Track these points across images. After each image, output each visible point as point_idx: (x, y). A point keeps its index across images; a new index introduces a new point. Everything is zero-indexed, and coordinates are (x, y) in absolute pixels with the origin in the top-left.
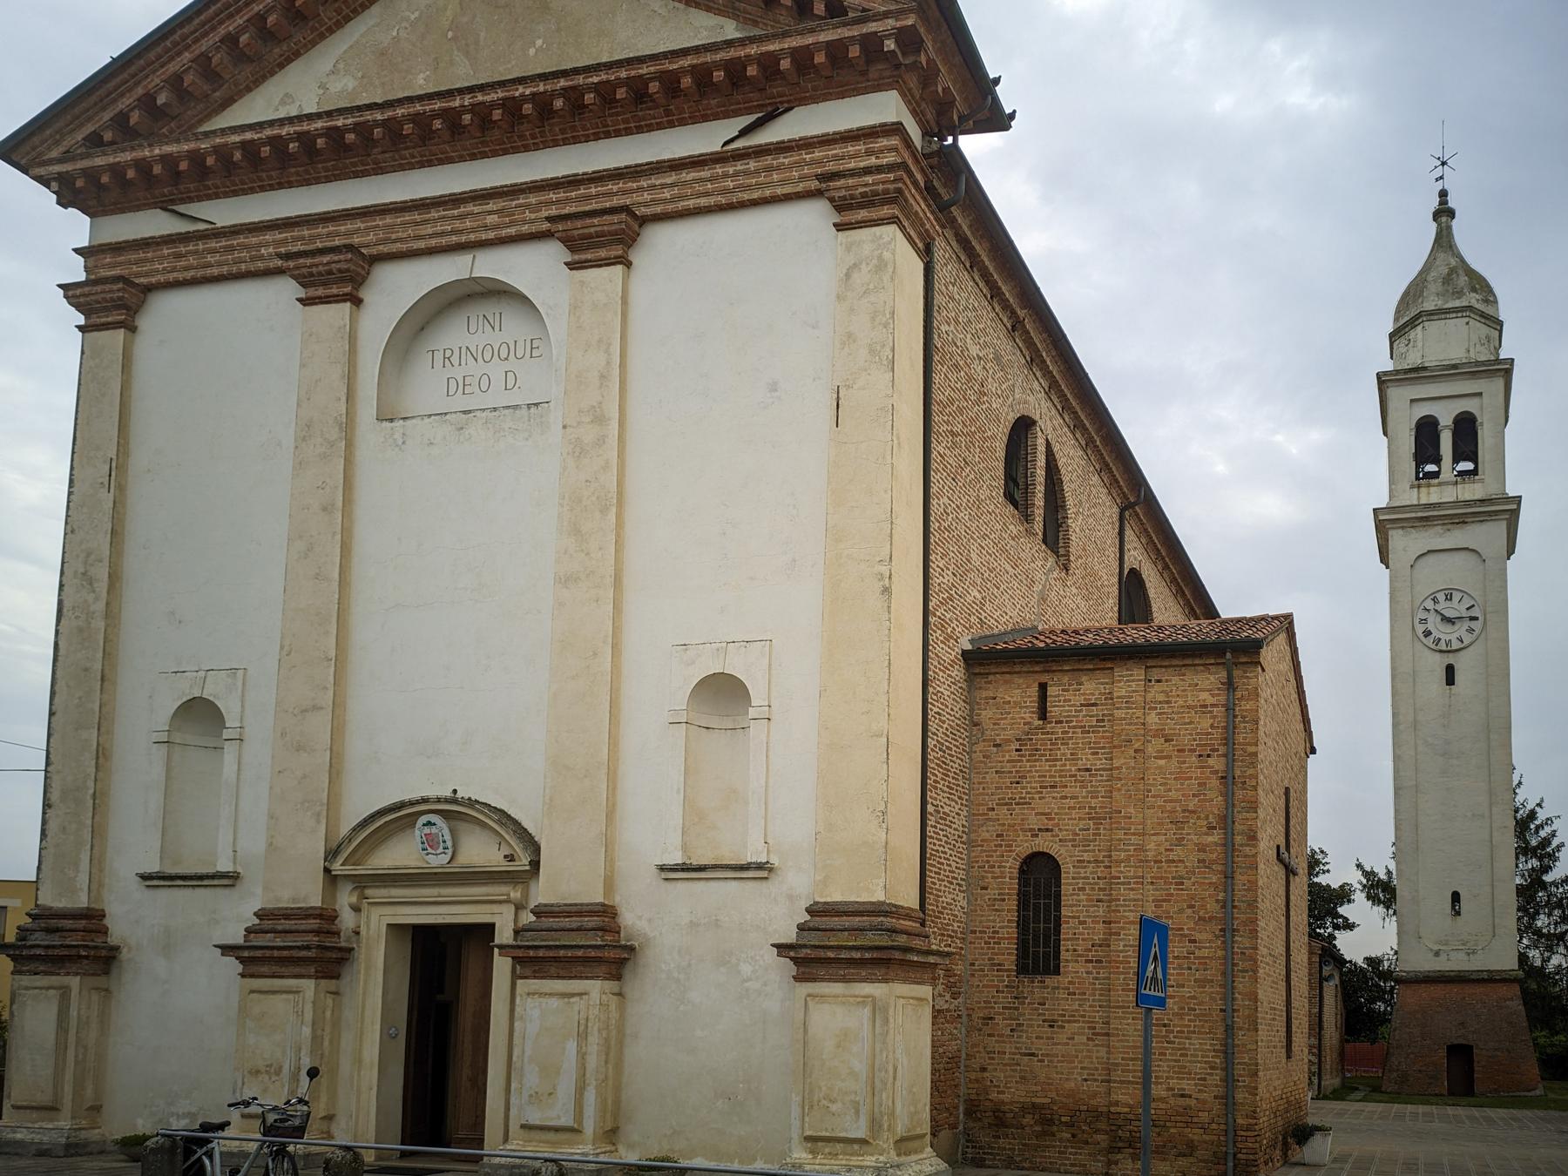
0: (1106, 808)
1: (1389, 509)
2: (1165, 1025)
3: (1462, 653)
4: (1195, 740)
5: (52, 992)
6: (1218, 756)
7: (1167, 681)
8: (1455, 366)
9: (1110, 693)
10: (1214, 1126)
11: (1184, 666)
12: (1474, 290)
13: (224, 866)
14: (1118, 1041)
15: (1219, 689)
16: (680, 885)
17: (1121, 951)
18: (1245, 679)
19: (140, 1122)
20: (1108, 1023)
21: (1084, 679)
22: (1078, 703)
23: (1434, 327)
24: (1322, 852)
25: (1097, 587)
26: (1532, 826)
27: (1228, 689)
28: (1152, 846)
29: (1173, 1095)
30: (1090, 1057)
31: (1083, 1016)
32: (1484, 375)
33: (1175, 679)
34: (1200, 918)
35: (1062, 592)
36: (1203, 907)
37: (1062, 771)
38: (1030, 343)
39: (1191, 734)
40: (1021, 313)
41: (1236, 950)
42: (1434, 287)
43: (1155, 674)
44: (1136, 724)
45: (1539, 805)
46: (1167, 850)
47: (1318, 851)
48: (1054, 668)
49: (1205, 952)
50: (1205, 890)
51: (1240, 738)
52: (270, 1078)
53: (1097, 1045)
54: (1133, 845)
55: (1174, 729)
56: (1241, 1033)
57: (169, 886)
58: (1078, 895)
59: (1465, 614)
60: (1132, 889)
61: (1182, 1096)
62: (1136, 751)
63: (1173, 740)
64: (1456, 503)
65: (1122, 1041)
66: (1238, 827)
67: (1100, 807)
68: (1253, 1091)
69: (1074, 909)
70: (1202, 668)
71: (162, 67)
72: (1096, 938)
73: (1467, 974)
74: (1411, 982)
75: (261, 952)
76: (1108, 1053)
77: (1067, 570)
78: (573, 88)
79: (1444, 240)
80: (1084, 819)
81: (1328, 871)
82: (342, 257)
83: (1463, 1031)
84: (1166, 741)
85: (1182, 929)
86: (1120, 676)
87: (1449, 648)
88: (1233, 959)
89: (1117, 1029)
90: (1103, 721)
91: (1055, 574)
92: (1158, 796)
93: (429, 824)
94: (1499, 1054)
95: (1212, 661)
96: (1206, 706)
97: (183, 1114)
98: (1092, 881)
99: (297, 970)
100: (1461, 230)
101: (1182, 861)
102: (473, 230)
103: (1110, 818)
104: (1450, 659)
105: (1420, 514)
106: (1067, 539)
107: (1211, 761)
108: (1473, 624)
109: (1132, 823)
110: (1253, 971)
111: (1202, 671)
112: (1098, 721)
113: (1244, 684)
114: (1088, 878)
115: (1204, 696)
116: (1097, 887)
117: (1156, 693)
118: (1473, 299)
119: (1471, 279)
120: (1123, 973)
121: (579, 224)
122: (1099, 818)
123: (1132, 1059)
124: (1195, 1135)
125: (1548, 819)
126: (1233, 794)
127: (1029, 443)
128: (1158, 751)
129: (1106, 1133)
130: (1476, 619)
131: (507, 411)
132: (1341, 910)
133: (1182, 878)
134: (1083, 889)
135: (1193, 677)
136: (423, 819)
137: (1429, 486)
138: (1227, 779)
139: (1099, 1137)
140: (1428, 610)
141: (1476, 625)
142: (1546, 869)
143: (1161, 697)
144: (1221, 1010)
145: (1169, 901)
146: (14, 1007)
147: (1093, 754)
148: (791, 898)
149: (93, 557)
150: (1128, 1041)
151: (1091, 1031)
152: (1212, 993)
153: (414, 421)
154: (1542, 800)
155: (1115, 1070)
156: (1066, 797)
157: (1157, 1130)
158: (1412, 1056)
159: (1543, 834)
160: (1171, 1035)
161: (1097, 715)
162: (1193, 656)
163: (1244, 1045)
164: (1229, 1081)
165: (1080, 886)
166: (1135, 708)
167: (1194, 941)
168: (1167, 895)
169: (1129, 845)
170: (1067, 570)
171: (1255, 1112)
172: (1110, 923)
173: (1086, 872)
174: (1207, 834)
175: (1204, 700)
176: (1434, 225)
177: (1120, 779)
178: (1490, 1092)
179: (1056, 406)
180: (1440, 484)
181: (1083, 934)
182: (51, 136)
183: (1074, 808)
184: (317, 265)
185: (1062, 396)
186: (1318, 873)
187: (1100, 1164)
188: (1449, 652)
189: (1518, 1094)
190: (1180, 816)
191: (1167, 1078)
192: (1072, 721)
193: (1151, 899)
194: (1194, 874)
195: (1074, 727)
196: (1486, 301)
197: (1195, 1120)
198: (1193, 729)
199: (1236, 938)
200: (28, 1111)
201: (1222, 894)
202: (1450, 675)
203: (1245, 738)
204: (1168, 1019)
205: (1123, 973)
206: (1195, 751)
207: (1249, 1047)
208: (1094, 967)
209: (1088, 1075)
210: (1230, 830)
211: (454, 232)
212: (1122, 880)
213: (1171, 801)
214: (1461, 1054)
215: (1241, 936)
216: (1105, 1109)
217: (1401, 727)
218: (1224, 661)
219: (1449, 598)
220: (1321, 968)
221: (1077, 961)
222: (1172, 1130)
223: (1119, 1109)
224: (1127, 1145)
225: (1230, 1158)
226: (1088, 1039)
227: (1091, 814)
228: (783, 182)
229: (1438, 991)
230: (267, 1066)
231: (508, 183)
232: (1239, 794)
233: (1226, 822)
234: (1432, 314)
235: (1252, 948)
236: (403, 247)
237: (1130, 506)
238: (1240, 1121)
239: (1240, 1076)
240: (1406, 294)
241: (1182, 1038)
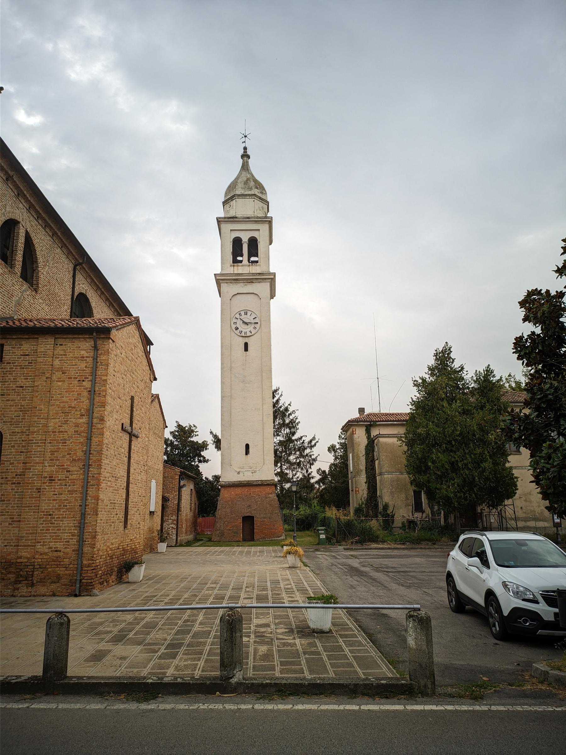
0: (29, 405)
1: (221, 275)
2: (50, 515)
3: (251, 337)
4: (77, 373)
6: (88, 381)
7: (65, 345)
8: (248, 218)
9: (36, 350)
10: (71, 566)
11: (74, 338)
12: (257, 188)
14: (25, 524)
15: (90, 349)
17: (30, 478)
18: (103, 345)
20: (20, 515)
21: (23, 342)
22: (19, 354)
23: (240, 201)
24: (194, 426)
25: (57, 300)
26: (287, 414)
27: (95, 349)
28: (52, 424)
29: (51, 551)
30: (9, 534)
31: (8, 512)
32: (261, 222)
33: (70, 344)
34: (73, 460)
35: (32, 301)
36: (75, 454)
37: (8, 387)
38: (17, 187)
39: (75, 370)
40: (11, 173)
41: (90, 475)
42: (240, 185)
43: (60, 341)
44: (48, 365)
45: (290, 405)
46: (59, 426)
47: (192, 426)
48: (8, 337)
49: (74, 477)
50: (77, 446)
51: (99, 373)
53: (14, 527)
54: (42, 424)
55: (68, 368)
56: (89, 516)
58: (11, 449)
59: (253, 321)
60: (39, 446)
61: (56, 551)
62: (47, 378)
63: (66, 373)
64: (249, 274)
65: (27, 524)
66: (95, 415)
67: (27, 405)
68: (93, 546)
69: (8, 457)
70: (83, 339)
72: (18, 471)
73: (252, 482)
74: (226, 487)
76: (19, 531)
77: (36, 291)
79: (245, 167)
80: (18, 411)
81: (198, 435)
84: (63, 373)
85: (64, 465)
86: (41, 342)
88: (88, 479)
89: (25, 518)
90: (32, 363)
91: (28, 293)
92: (57, 400)
94: (265, 520)
95: (88, 336)
96: (84, 357)
98: (19, 442)
100: (251, 162)
101: (66, 432)
103: (31, 411)
104: (246, 340)
105: (234, 278)
106: (38, 277)
107: (84, 383)
108: (256, 326)
109: (42, 413)
110: (97, 485)
111: (83, 341)
112: (29, 363)
113: (102, 347)
114: (17, 441)
115: (83, 352)
116: (21, 445)
117: (59, 350)
118: (256, 192)
119: (255, 183)
120: (31, 489)
122: (26, 411)
123: (31, 534)
124: (61, 571)
125: (293, 411)
126: (94, 399)
127: (16, 231)
128: (59, 378)
129: (14, 573)
130: (257, 323)
132: (202, 453)
133: (65, 440)
134: (14, 446)
135: (78, 343)
137: (238, 266)
138: (92, 392)
139: (10, 576)
140: (237, 319)
141: (257, 326)
142: (294, 434)
143: (62, 353)
144: (80, 506)
145: (58, 451)
147: (25, 379)
150: (30, 524)
151: (11, 520)
152: (76, 497)
154: (291, 403)
155: (22, 540)
156: (9, 400)
157: (41, 570)
158: (226, 523)
159: (291, 417)
160: (53, 520)
161: (29, 360)
162: (79, 334)
163: (90, 523)
164: (81, 541)
165: (12, 445)
166: (48, 357)
167: (69, 471)
168: (57, 449)
169: (39, 424)
170: (36, 291)
171: (93, 557)
172: (26, 463)
173: (16, 438)
174: (80, 418)
175: (83, 355)
176: (242, 160)
177: (38, 392)
178: (261, 539)
179: (33, 216)
180: (242, 266)
181: (12, 469)
183: (13, 406)
185: (37, 211)
186: (193, 436)
187: (9, 591)
188: (246, 337)
189: (274, 539)
190: (67, 410)
191: (49, 542)
192: (15, 363)
193: (49, 451)
194: (72, 437)
195: (16, 366)
196: (262, 193)
197: (62, 563)
198: (77, 368)
199: (91, 469)
201: (85, 447)
202: (246, 346)
203: (101, 373)
204: (52, 512)
205: (31, 489)
206: (77, 378)
207: (92, 523)
208: (16, 487)
209: (8, 543)
210: (91, 416)
212: (34, 441)
213: (63, 402)
214: (248, 520)
215: (93, 468)
216: (15, 561)
217: (225, 369)
218: (92, 336)
219: (246, 314)
220: (180, 481)
221: (7, 484)
222: (49, 570)
223: (22, 560)
224: (24, 579)
225: (78, 582)
226: (9, 524)
227: (21, 408)
229: (239, 490)
232: (97, 399)
233: (90, 412)
234: (239, 196)
235: (98, 474)
237: (80, 264)
238: (85, 562)
239: (87, 539)
240: (229, 187)
241: (59, 521)
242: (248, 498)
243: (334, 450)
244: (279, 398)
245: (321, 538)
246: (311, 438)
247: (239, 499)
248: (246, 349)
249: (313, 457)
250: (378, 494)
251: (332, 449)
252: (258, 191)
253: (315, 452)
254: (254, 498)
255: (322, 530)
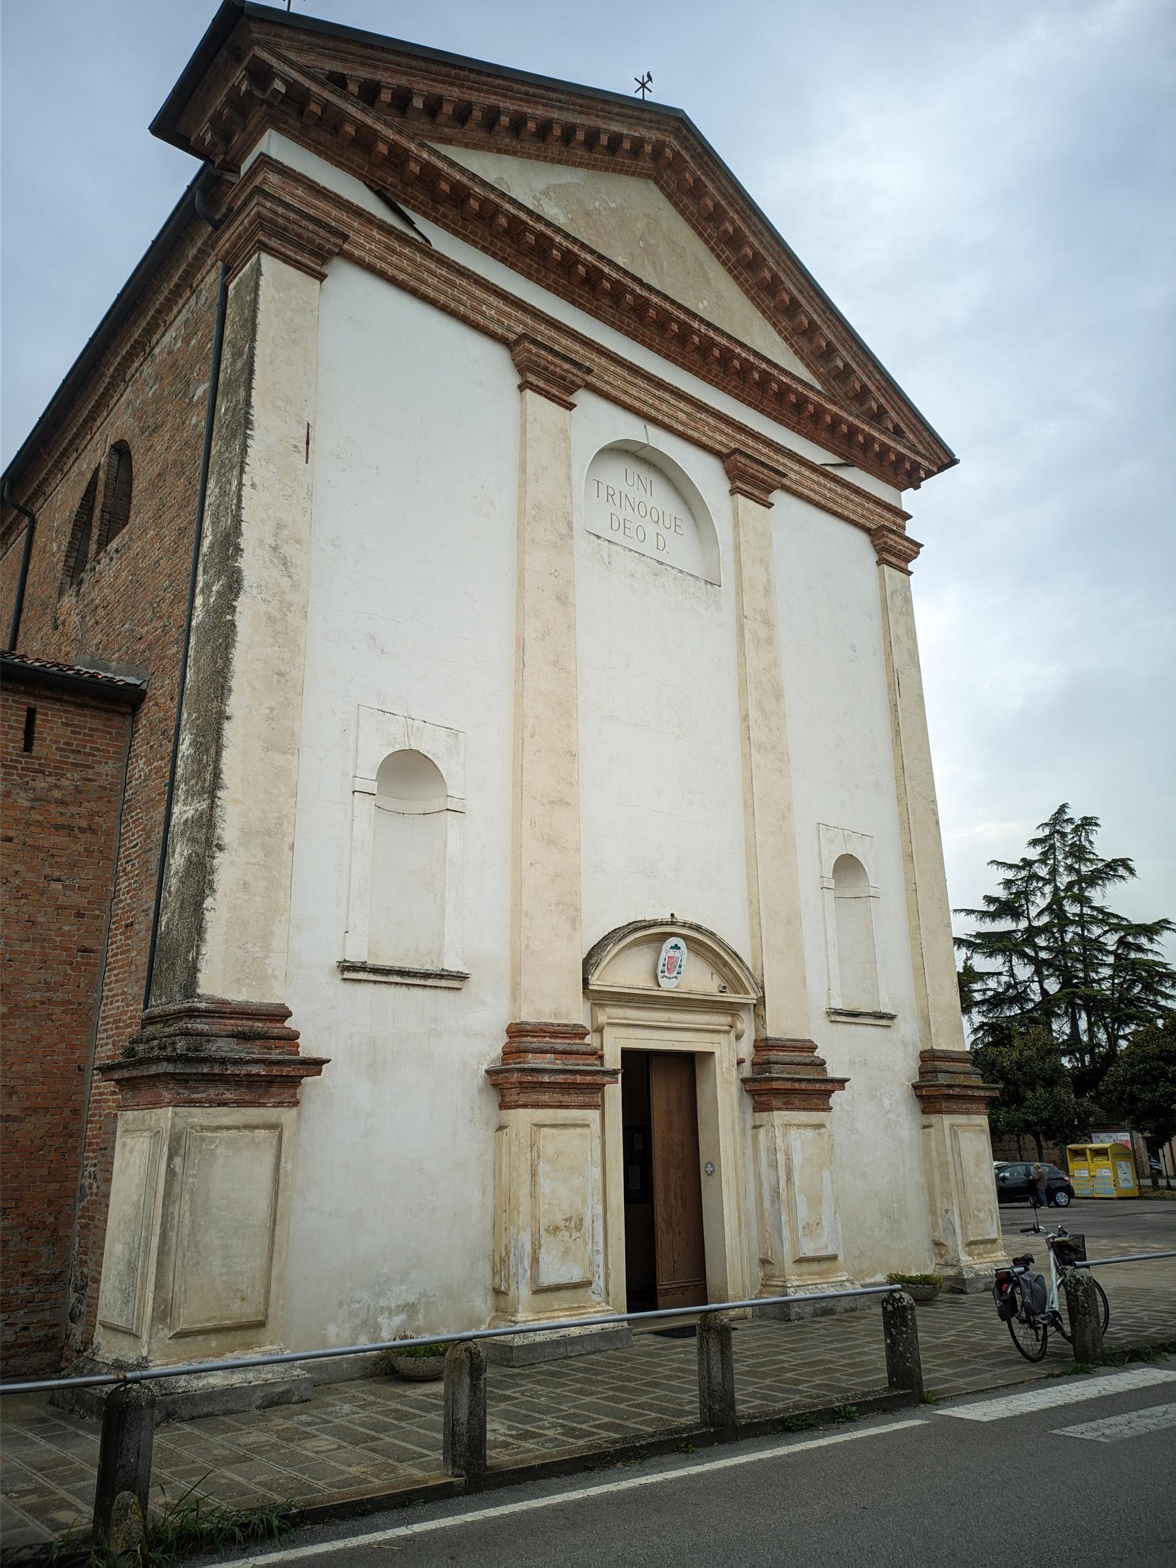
5: (262, 1134)
13: (452, 964)
16: (840, 1026)
19: (332, 1330)
52: (571, 1236)
57: (375, 982)
71: (432, 80)
75: (563, 1077)
78: (770, 374)
82: (580, 374)
93: (676, 947)
97: (398, 1306)
99: (582, 1099)
102: (668, 415)
121: (755, 466)
131: (689, 577)
136: (672, 941)
146: (178, 1160)
148: (904, 1044)
149: (286, 532)
153: (616, 547)
182: (302, 42)
184: (556, 366)
200: (201, 1338)
211: (652, 406)
228: (854, 512)
230: (566, 1220)
231: (704, 401)
236: (606, 388)
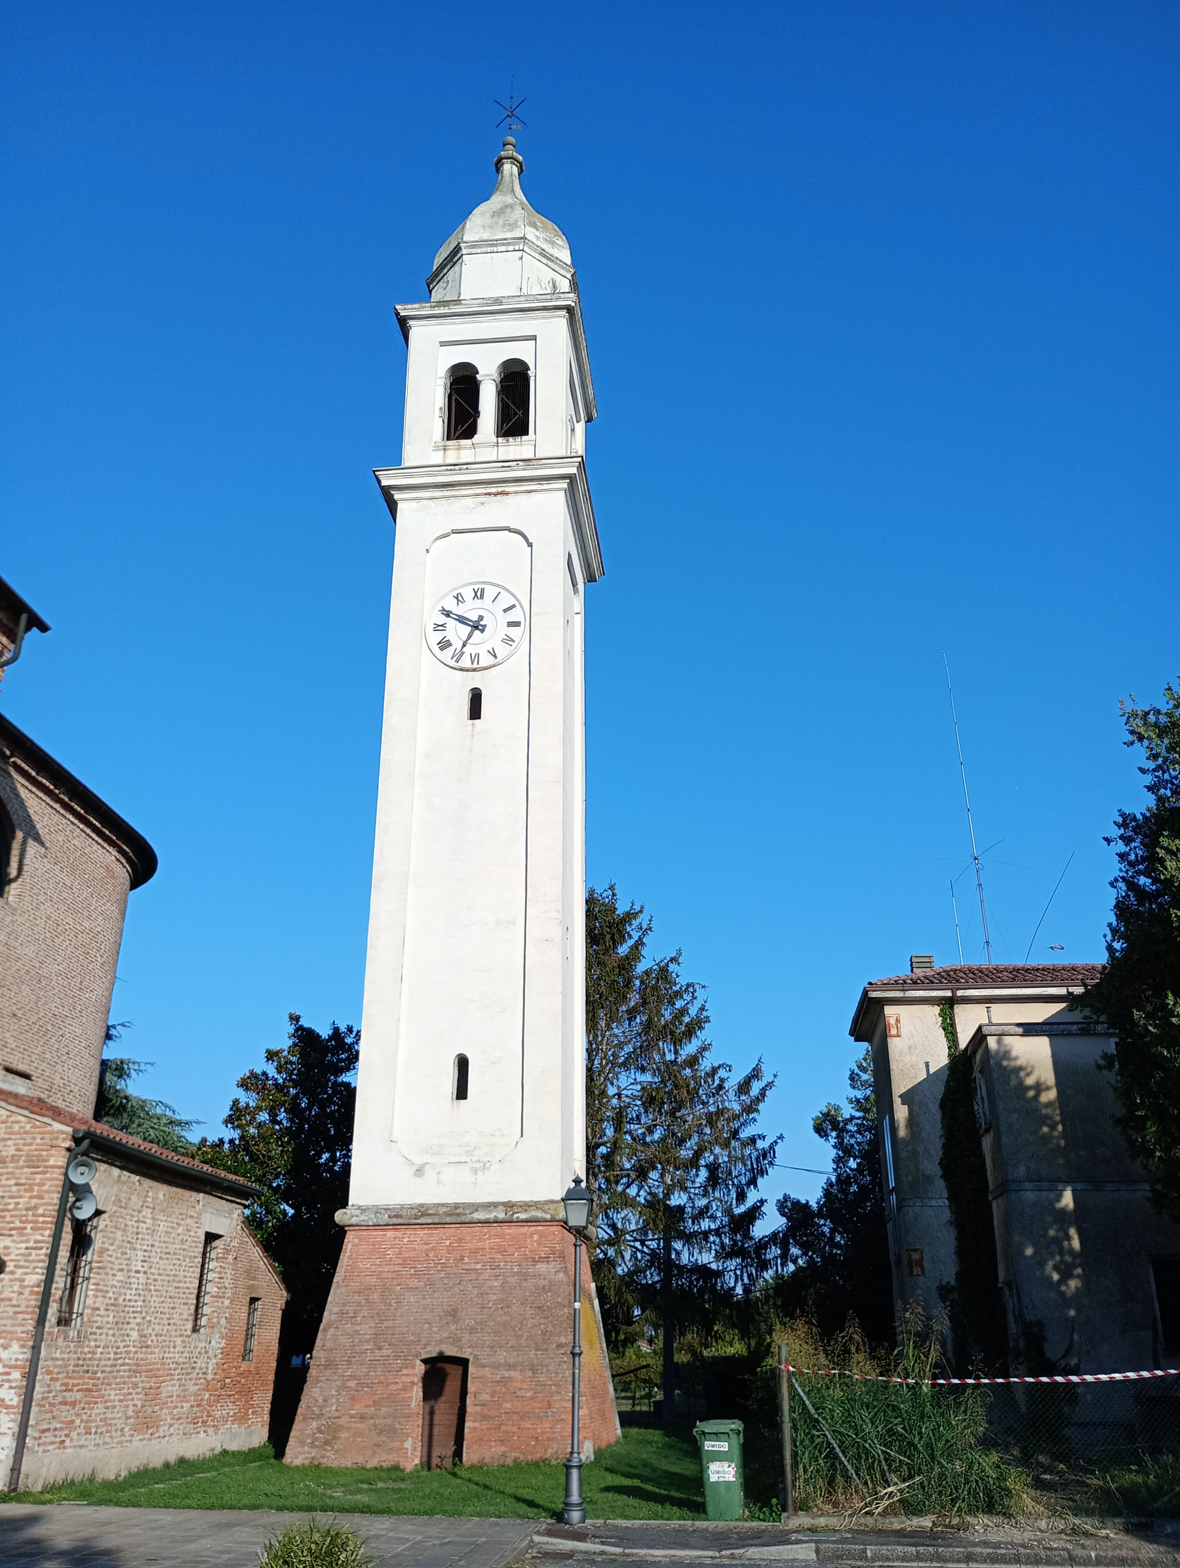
83: (453, 1327)
87: (475, 665)
125: (689, 985)
130: (517, 624)
154: (679, 953)
158: (352, 1384)
188: (474, 670)
219: (479, 595)
242: (448, 1277)
243: (835, 1125)
244: (640, 939)
245: (713, 1478)
246: (747, 1071)
247: (414, 1282)
248: (475, 711)
249: (760, 1144)
250: (1001, 1275)
251: (827, 1124)
252: (537, 233)
253: (763, 1125)
254: (473, 1276)
255: (717, 1436)
